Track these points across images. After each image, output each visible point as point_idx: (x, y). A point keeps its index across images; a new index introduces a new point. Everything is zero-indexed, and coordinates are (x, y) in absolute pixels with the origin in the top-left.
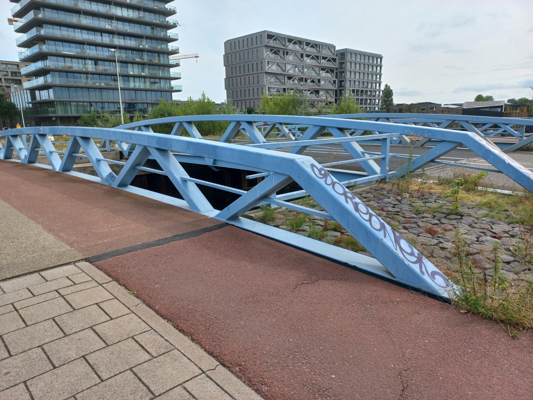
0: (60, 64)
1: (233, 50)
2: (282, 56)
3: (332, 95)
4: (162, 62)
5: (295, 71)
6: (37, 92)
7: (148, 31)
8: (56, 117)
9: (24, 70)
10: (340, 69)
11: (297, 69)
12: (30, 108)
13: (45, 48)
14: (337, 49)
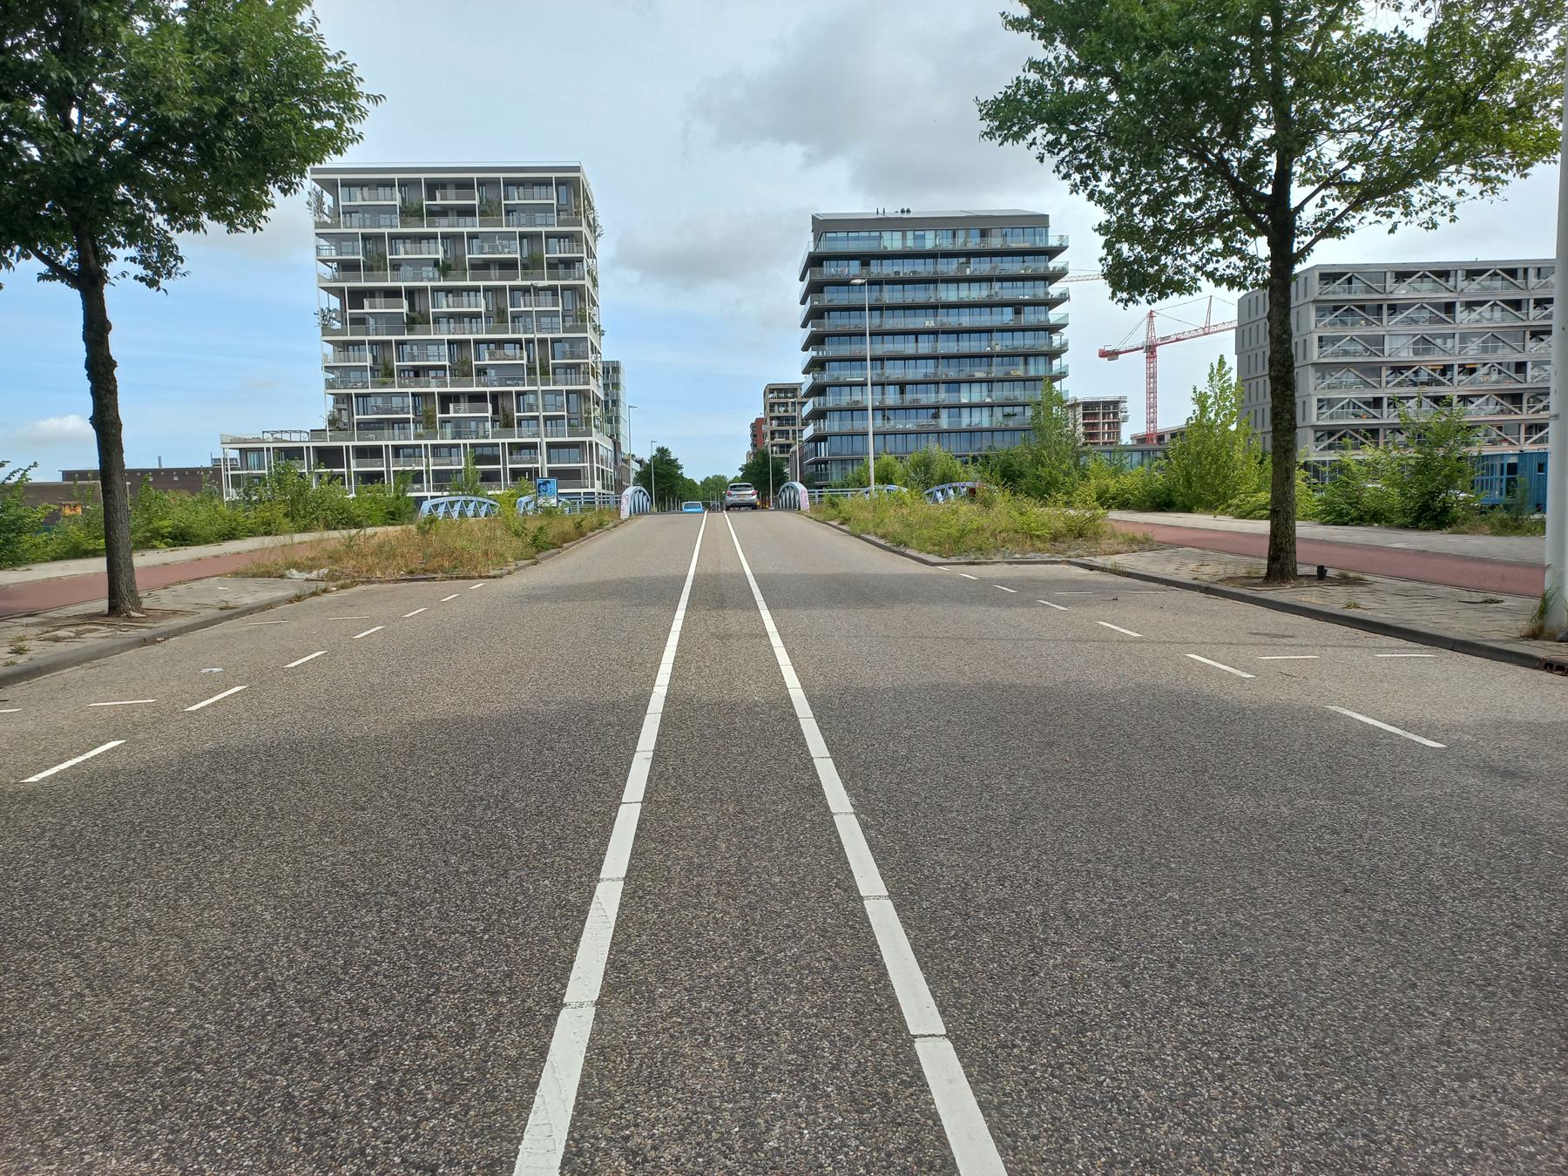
7: (1007, 316)
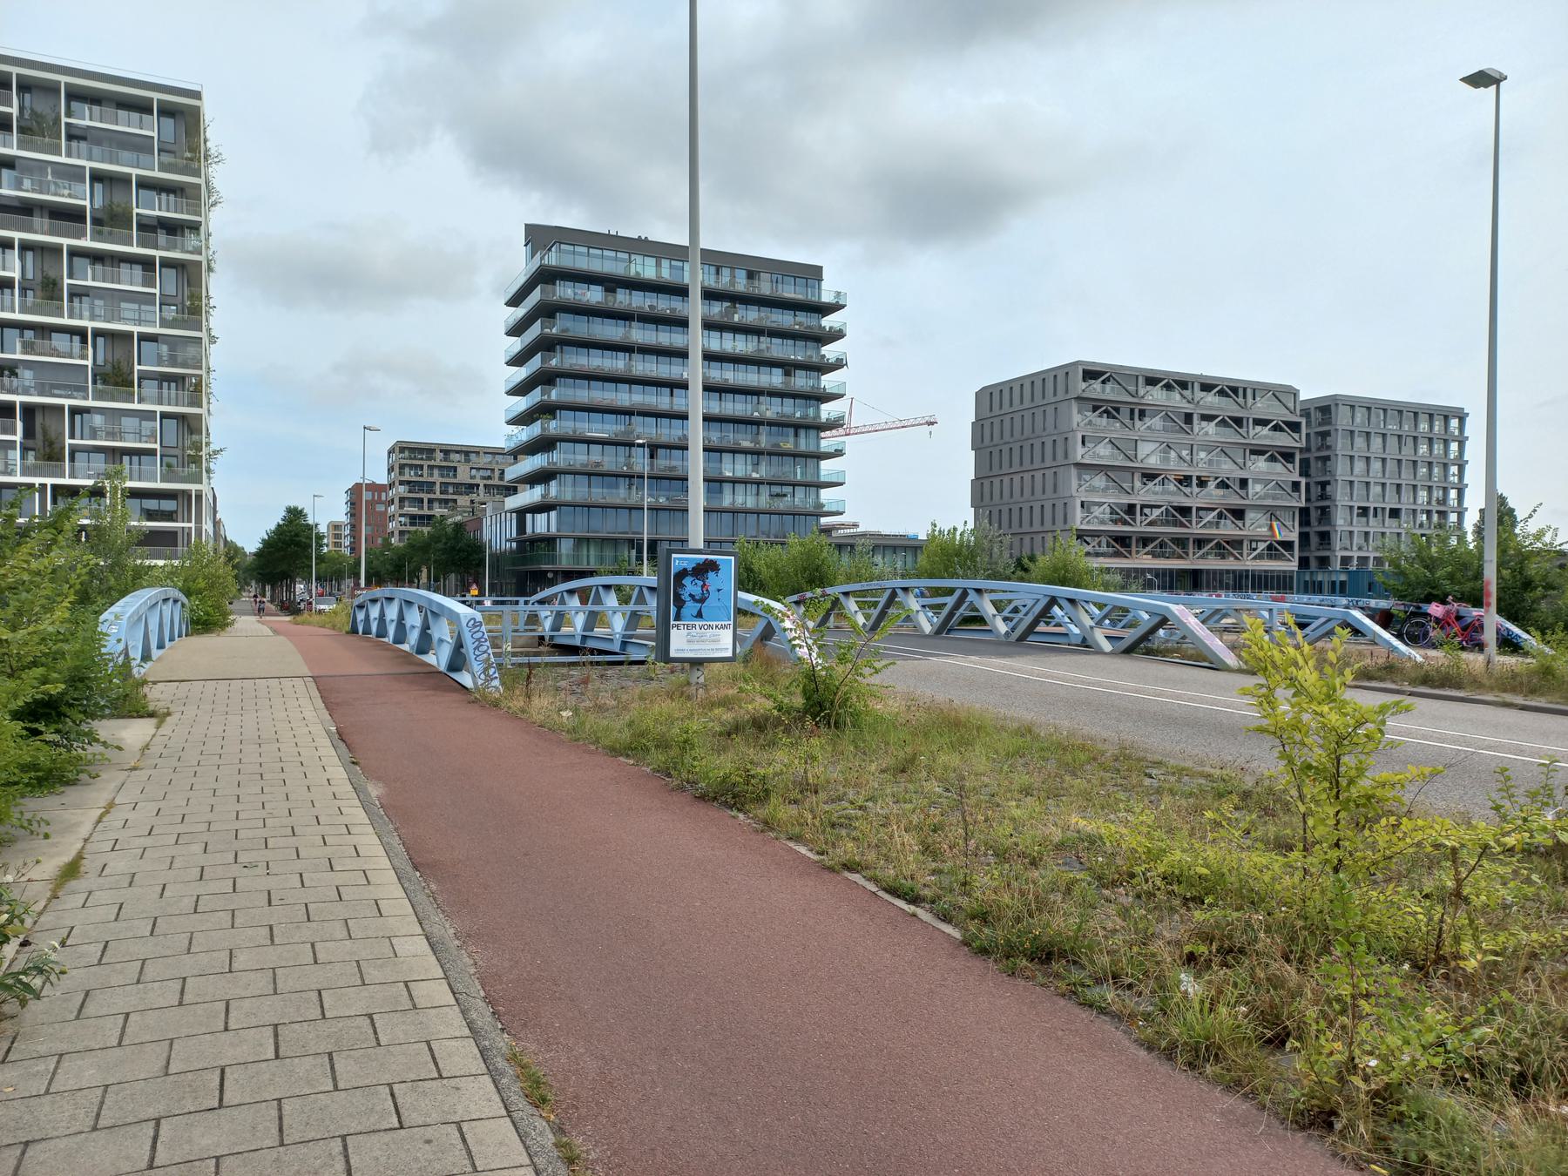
0: (579, 457)
1: (996, 411)
2: (1127, 421)
3: (1289, 524)
4: (803, 447)
5: (1166, 459)
6: (529, 516)
7: (776, 379)
8: (556, 573)
9: (516, 470)
10: (1319, 449)
11: (1173, 454)
12: (511, 551)
13: (553, 427)
14: (1303, 396)
